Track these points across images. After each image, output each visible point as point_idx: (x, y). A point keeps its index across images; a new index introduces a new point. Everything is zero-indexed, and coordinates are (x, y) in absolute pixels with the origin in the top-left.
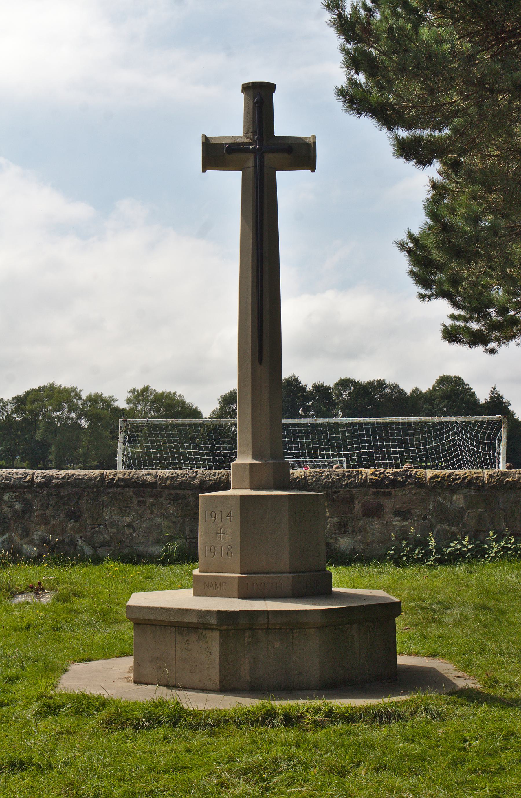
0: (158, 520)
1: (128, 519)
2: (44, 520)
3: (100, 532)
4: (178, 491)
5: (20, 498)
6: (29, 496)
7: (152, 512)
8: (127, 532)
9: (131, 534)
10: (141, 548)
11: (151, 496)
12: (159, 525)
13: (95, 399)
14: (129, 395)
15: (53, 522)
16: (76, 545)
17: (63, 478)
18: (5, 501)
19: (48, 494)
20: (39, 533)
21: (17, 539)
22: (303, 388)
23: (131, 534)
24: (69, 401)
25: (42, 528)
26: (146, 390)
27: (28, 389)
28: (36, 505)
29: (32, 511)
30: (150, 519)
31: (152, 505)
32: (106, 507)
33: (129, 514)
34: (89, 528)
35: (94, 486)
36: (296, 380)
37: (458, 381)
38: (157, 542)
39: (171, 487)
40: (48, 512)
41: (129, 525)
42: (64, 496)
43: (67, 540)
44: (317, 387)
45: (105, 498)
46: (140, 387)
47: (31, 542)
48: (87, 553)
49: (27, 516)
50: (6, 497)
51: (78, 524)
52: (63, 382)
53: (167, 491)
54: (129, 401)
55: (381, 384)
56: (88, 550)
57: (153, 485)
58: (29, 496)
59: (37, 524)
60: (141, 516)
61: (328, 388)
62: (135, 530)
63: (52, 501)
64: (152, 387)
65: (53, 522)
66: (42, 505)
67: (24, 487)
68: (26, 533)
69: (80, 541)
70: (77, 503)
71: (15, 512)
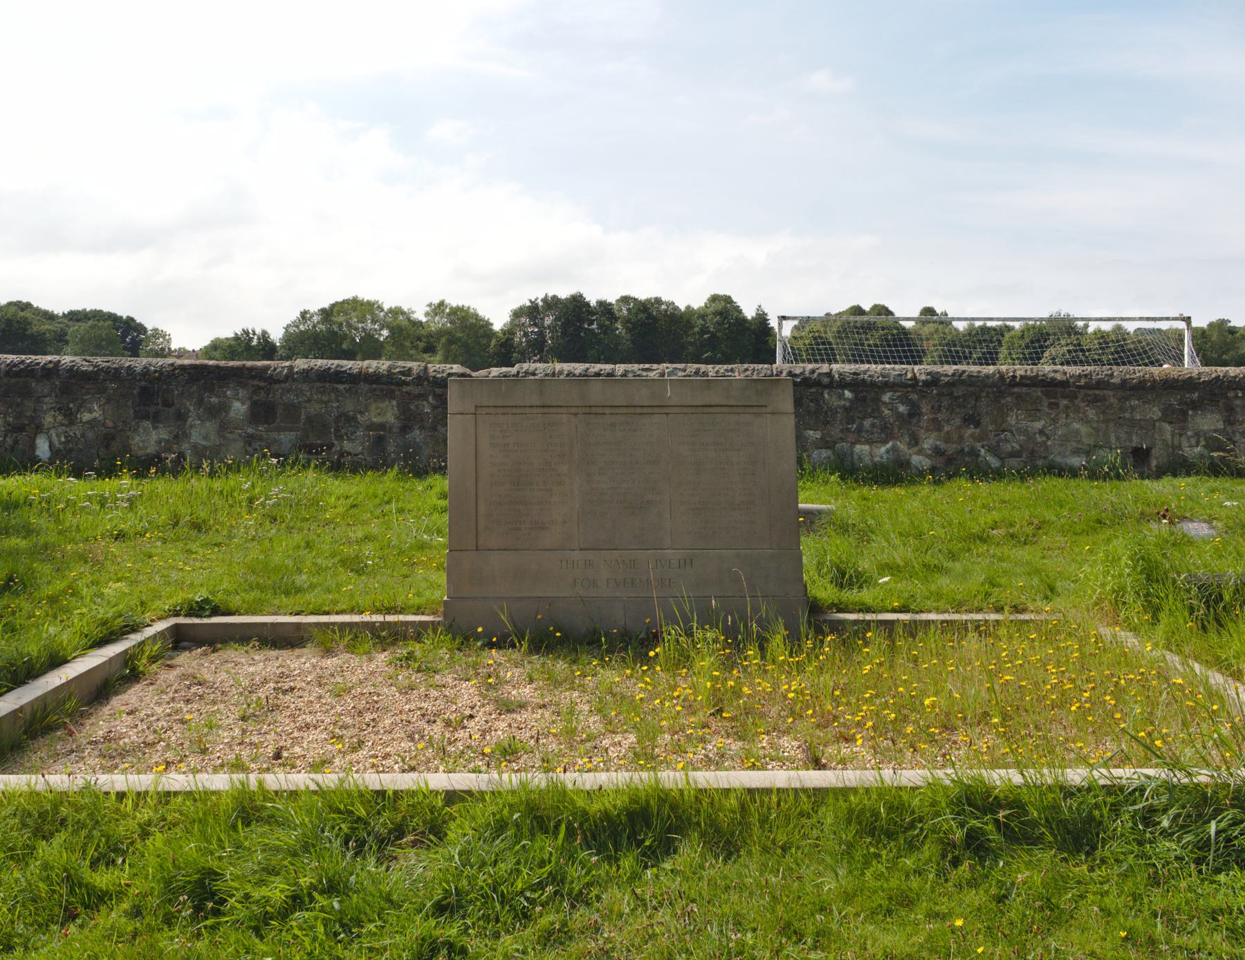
0: (1076, 425)
1: (1038, 425)
2: (936, 425)
3: (1006, 441)
4: (1097, 392)
5: (904, 400)
6: (914, 397)
7: (1067, 416)
8: (1039, 440)
9: (1044, 442)
10: (1058, 459)
11: (1064, 397)
12: (1077, 432)
13: (397, 312)
14: (428, 309)
15: (947, 428)
16: (978, 456)
17: (953, 375)
18: (885, 403)
19: (939, 395)
20: (931, 441)
21: (902, 446)
22: (588, 304)
23: (1044, 442)
24: (372, 314)
25: (934, 434)
26: (442, 304)
27: (333, 302)
28: (925, 408)
29: (920, 414)
30: (1067, 425)
31: (1067, 407)
32: (1011, 409)
33: (1040, 419)
34: (991, 436)
35: (994, 385)
36: (581, 296)
37: (728, 300)
38: (1076, 452)
39: (1088, 386)
40: (940, 416)
41: (1041, 432)
42: (959, 397)
43: (967, 449)
44: (601, 304)
45: (1009, 399)
46: (436, 301)
47: (920, 452)
48: (38, 453)
49: (914, 421)
50: (886, 397)
51: (978, 430)
52: (366, 295)
53: (1083, 392)
54: (427, 314)
55: (658, 301)
56: (994, 462)
57: (1064, 384)
58: (914, 397)
59: (928, 430)
60: (1055, 421)
61: (610, 304)
62: (1048, 438)
63: (945, 403)
64: (447, 301)
65: (947, 428)
66: (933, 407)
67: (907, 386)
68: (915, 441)
69: (983, 451)
70: (975, 406)
71: (899, 416)
